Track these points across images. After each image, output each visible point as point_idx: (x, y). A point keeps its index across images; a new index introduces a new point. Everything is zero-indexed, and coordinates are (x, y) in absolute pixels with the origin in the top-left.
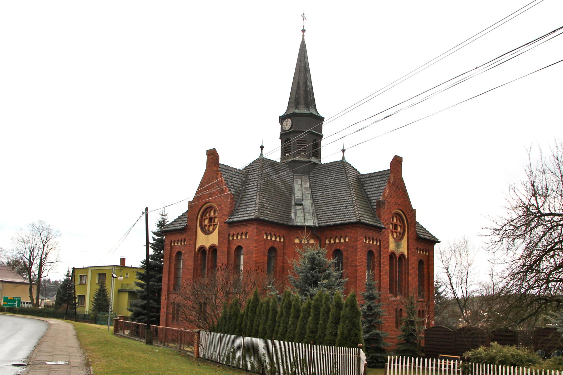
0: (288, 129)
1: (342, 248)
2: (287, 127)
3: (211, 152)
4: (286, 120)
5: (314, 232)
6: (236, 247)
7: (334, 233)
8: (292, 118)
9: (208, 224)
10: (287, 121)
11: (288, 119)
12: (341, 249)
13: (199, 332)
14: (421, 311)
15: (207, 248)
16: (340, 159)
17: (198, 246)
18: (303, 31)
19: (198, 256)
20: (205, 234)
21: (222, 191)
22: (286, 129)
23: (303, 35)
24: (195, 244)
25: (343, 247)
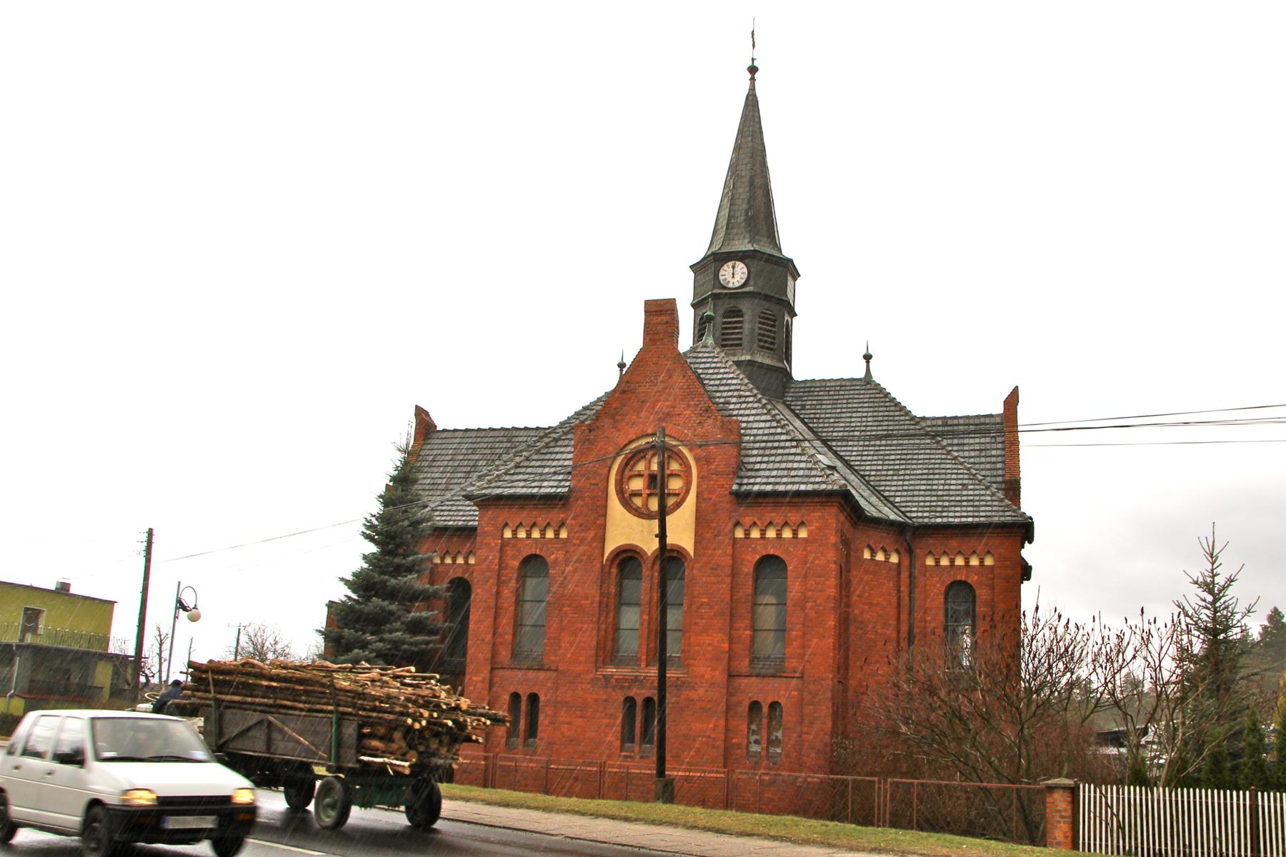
0: (737, 285)
1: (973, 579)
2: (735, 280)
3: (661, 305)
4: (730, 264)
5: (907, 538)
6: (758, 557)
7: (954, 543)
8: (747, 261)
9: (648, 492)
10: (733, 267)
11: (737, 263)
12: (969, 581)
13: (1074, 791)
14: (765, 709)
15: (649, 554)
16: (861, 374)
17: (610, 547)
18: (753, 70)
19: (610, 573)
20: (639, 517)
21: (707, 410)
22: (730, 285)
23: (753, 79)
24: (602, 540)
25: (976, 577)
